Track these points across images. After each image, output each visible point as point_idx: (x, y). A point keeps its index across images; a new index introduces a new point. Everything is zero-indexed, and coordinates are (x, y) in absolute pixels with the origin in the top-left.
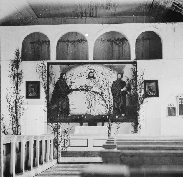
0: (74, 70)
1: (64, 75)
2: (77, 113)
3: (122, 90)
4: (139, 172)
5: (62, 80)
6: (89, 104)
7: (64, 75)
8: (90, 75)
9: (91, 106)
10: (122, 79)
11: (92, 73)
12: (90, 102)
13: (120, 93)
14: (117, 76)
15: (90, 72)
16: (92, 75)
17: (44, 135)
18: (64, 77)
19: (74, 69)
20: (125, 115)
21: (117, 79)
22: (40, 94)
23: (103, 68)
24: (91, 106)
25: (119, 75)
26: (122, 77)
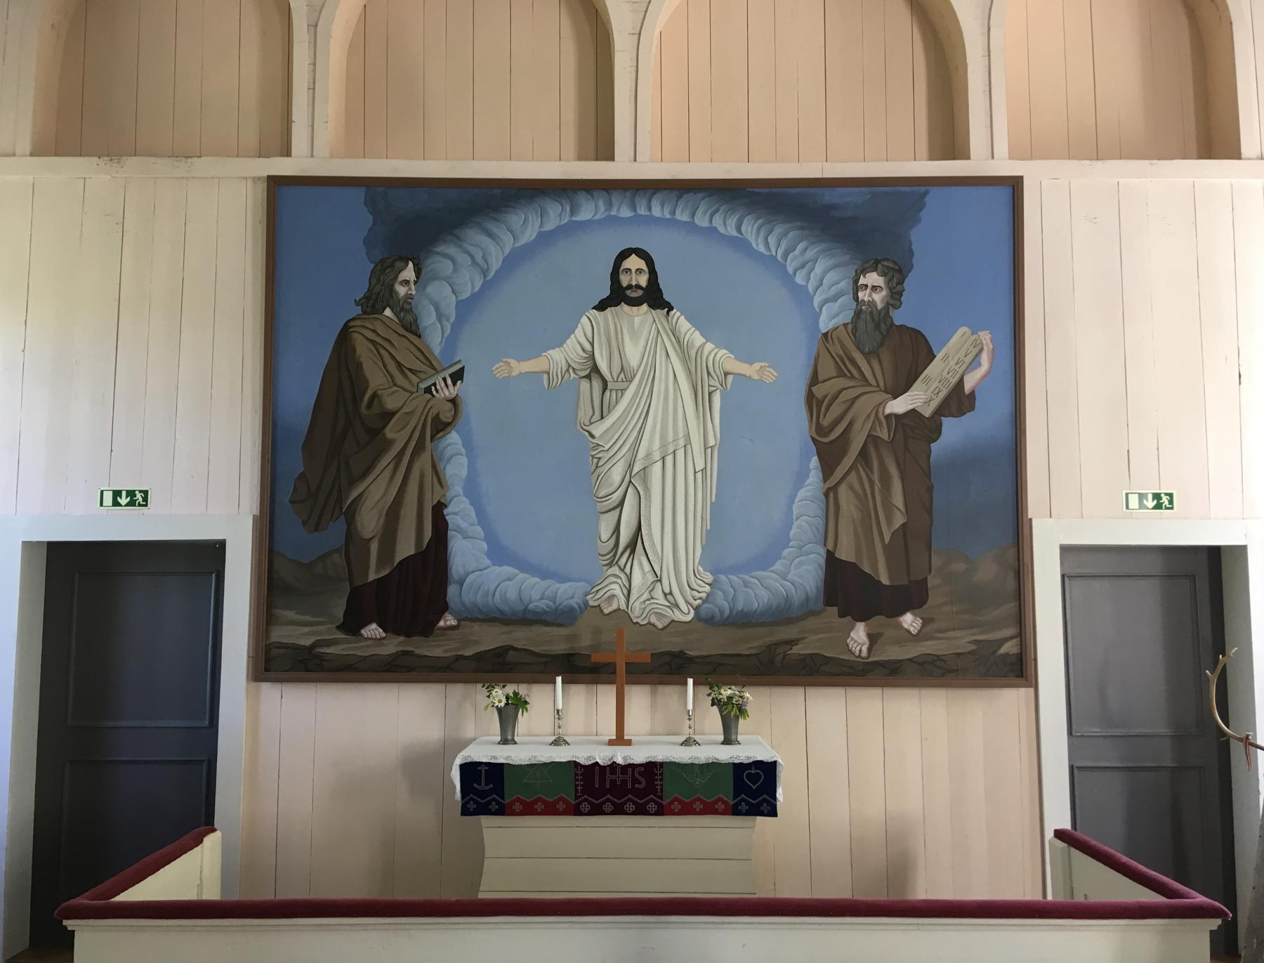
0: (490, 235)
1: (409, 273)
2: (512, 595)
3: (899, 406)
4: (740, 606)
5: (388, 312)
6: (617, 529)
7: (409, 273)
8: (624, 280)
9: (632, 546)
10: (898, 317)
11: (642, 264)
12: (621, 504)
13: (884, 434)
14: (856, 288)
15: (624, 255)
16: (643, 280)
17: (1220, 667)
18: (402, 291)
19: (491, 226)
20: (926, 622)
21: (858, 314)
22: (400, 526)
23: (732, 221)
24: (632, 546)
25: (873, 278)
26: (896, 295)
